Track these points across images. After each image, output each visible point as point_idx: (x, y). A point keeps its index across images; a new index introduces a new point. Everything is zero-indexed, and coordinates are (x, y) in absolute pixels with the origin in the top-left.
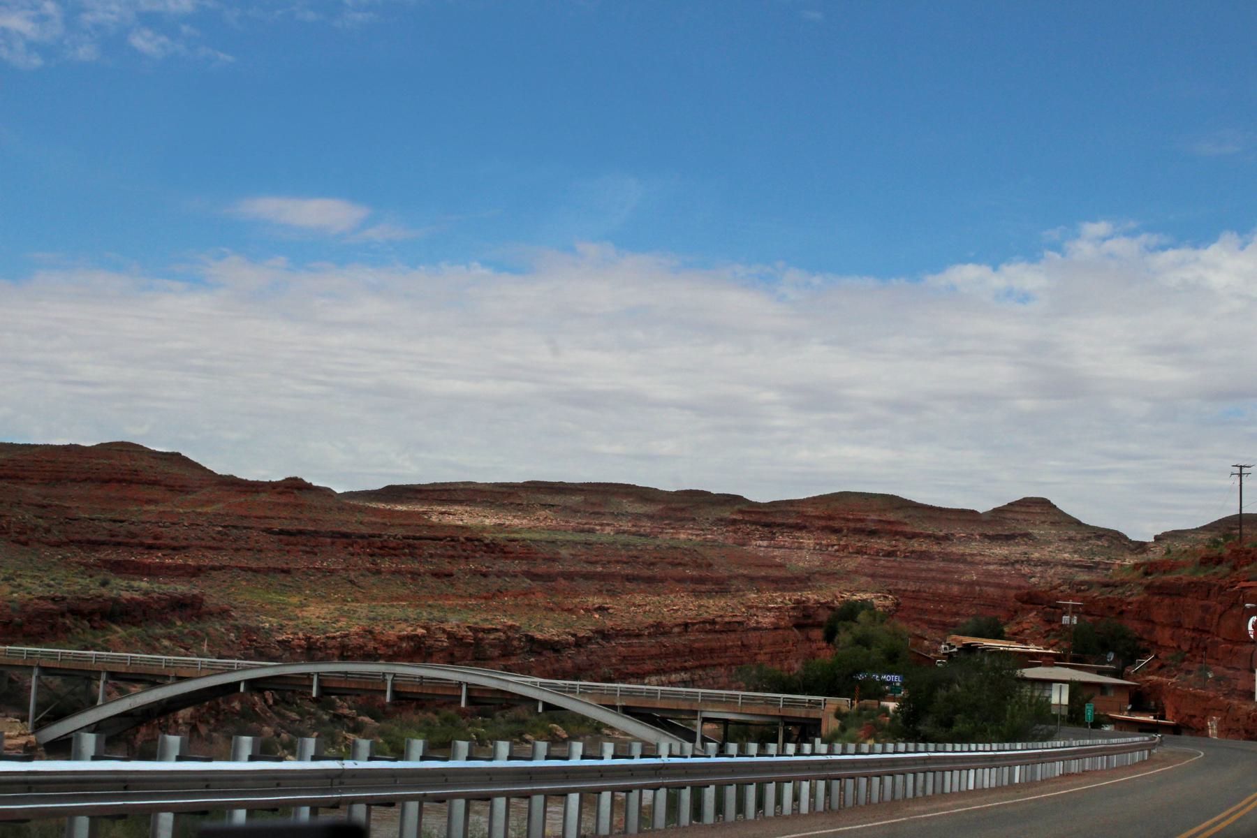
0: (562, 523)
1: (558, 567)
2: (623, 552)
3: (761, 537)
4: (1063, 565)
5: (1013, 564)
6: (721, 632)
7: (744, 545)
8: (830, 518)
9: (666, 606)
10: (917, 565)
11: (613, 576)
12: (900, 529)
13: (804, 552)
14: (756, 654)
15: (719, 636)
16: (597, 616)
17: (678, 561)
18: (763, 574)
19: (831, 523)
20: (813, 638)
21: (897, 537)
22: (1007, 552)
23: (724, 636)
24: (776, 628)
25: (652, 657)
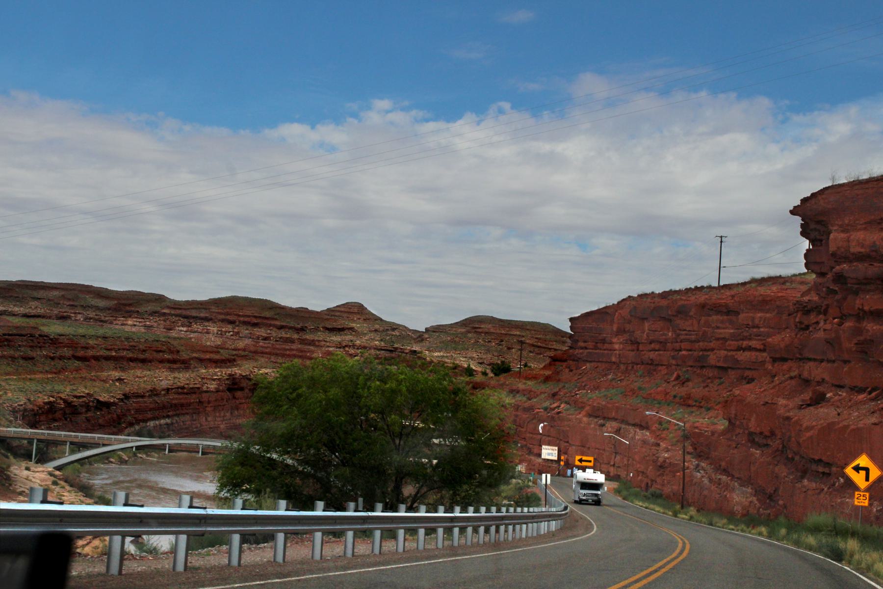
0: (48, 311)
1: (90, 353)
2: (126, 343)
3: (182, 325)
4: (375, 349)
5: (344, 347)
6: (187, 394)
7: (171, 329)
8: (228, 314)
9: (155, 378)
10: (284, 346)
11: (122, 358)
12: (273, 322)
13: (211, 336)
14: (206, 407)
15: (187, 396)
16: (118, 384)
17: (159, 349)
18: (473, 445)
19: (228, 317)
20: (237, 397)
21: (271, 328)
22: (340, 339)
23: (189, 396)
24: (217, 391)
25: (151, 410)
